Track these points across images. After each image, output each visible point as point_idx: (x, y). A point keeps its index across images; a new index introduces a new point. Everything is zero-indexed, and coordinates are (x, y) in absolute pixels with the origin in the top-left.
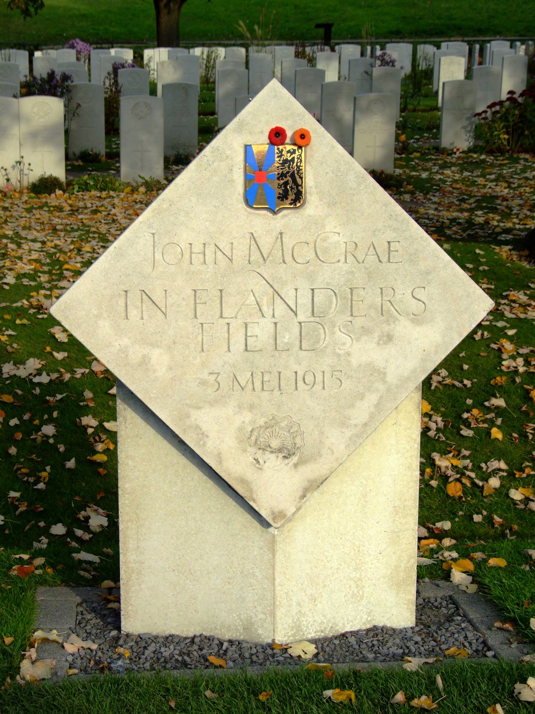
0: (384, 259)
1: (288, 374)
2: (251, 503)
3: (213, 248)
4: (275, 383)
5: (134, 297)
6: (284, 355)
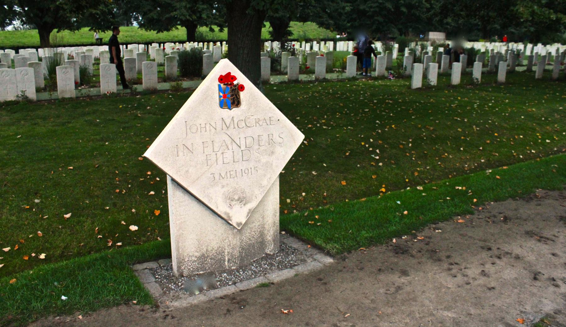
0: (268, 123)
1: (239, 170)
2: (230, 222)
3: (209, 125)
4: (234, 175)
5: (181, 148)
6: (237, 163)
